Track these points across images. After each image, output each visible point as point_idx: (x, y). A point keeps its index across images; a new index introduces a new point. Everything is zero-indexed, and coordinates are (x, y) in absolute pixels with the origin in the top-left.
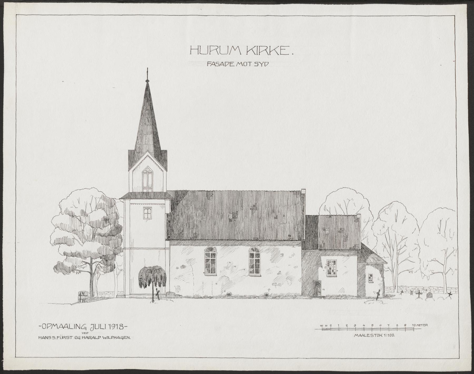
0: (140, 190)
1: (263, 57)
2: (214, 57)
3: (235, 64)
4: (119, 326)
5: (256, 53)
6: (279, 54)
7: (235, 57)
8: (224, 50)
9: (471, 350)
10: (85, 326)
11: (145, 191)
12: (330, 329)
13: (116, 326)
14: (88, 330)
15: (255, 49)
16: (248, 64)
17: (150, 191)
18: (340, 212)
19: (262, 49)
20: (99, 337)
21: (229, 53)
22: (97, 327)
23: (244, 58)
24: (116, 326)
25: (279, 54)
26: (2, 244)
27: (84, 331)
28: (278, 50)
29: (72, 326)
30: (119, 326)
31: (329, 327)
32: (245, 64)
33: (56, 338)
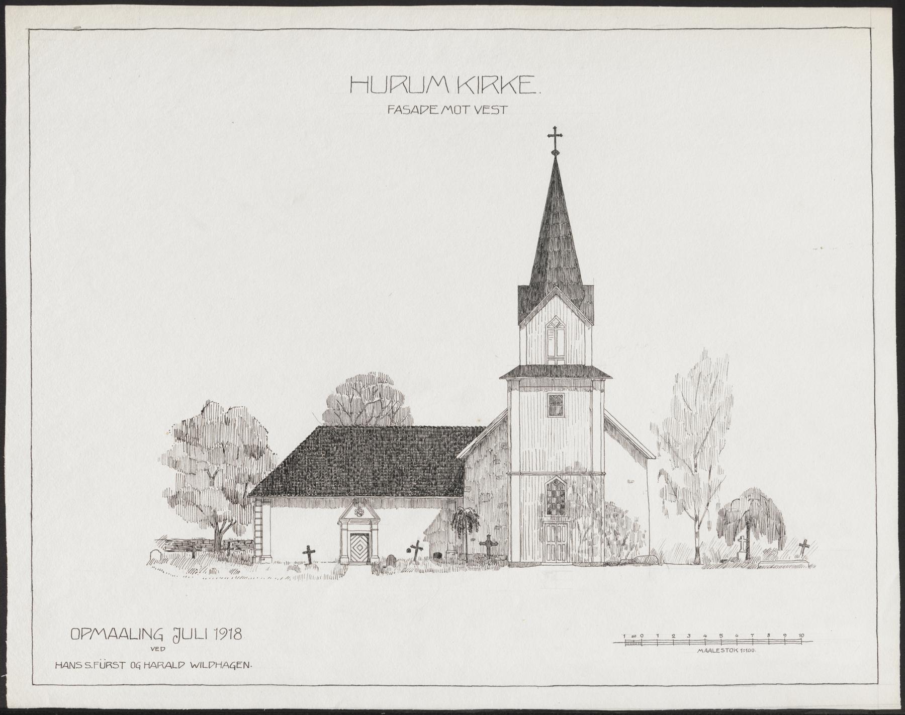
0: (541, 362)
1: (490, 97)
2: (399, 97)
3: (438, 110)
4: (234, 633)
5: (475, 92)
6: (517, 91)
7: (437, 96)
8: (416, 85)
9: (899, 625)
10: (160, 632)
11: (551, 363)
12: (641, 643)
13: (229, 632)
14: (168, 642)
15: (473, 84)
16: (463, 109)
17: (561, 363)
18: (382, 423)
19: (487, 81)
20: (181, 664)
21: (425, 90)
22: (187, 634)
23: (454, 99)
24: (229, 632)
25: (517, 91)
26: (3, 464)
27: (158, 643)
28: (516, 84)
29: (135, 634)
30: (234, 633)
31: (638, 638)
32: (458, 109)
33: (92, 665)
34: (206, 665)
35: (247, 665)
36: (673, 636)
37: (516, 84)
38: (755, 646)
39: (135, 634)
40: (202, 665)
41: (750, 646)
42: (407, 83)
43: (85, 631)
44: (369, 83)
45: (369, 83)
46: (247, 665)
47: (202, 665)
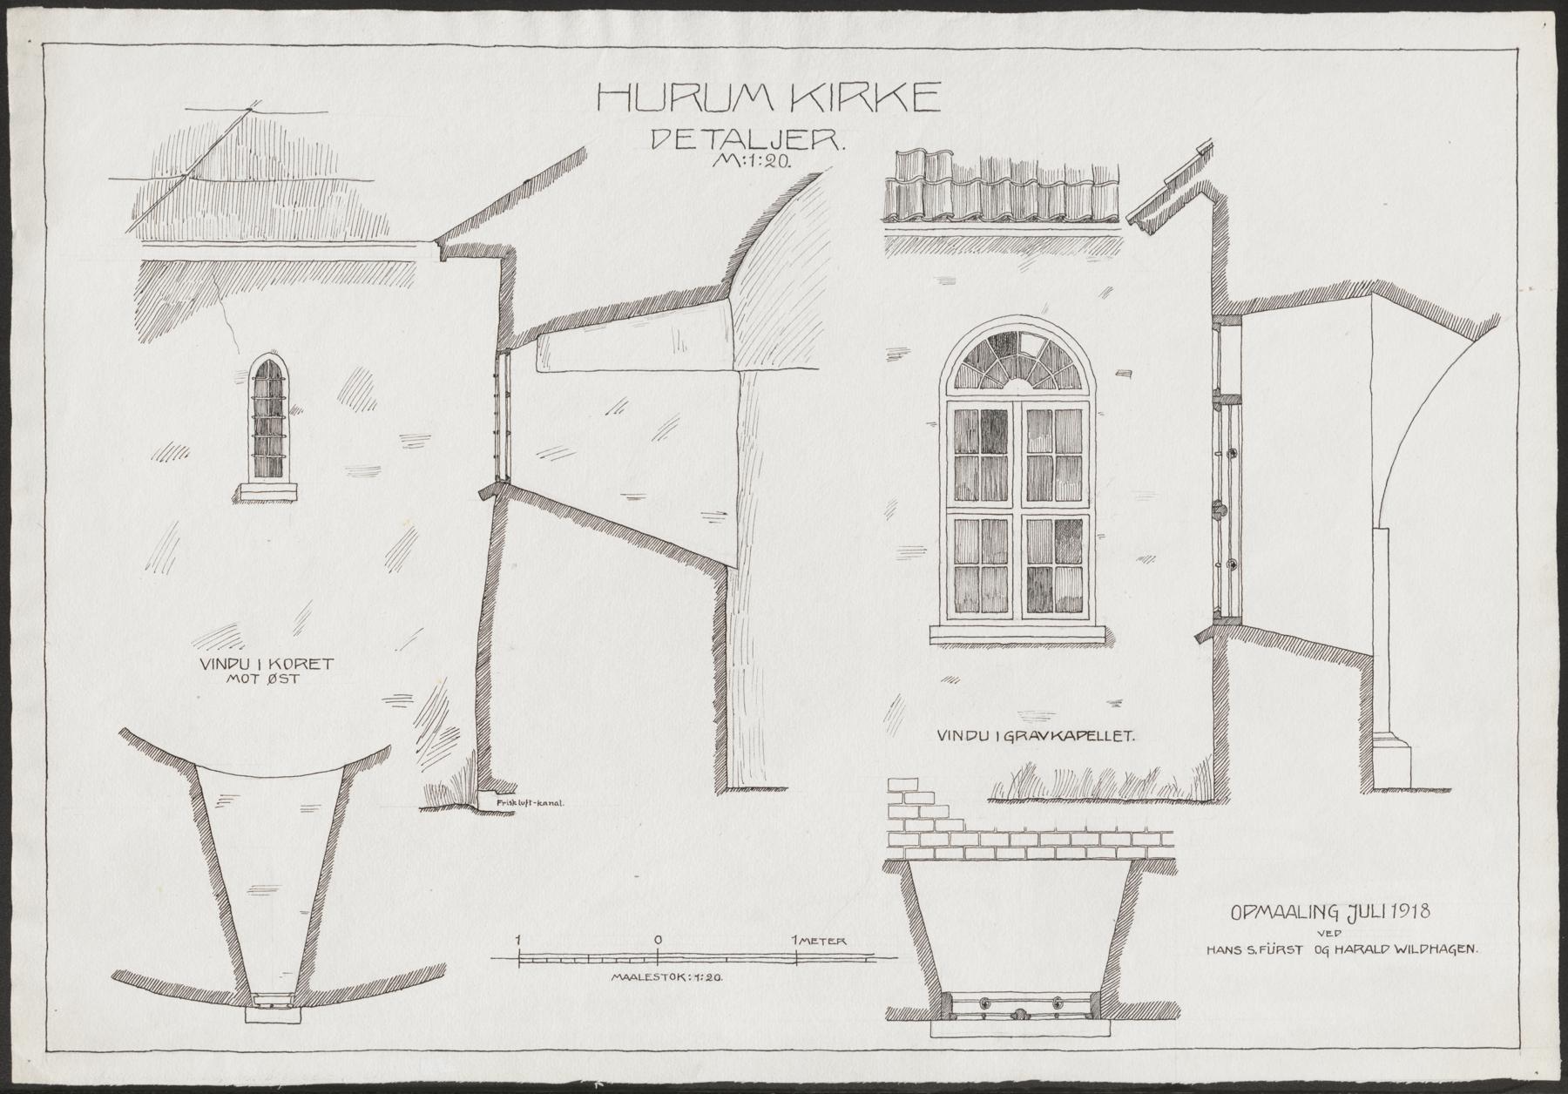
4: (1419, 909)
5: (826, 106)
8: (717, 100)
15: (823, 96)
25: (910, 105)
30: (1419, 909)
34: (1417, 949)
35: (1471, 948)
36: (658, 939)
37: (906, 93)
38: (791, 948)
39: (1305, 912)
40: (1410, 949)
41: (804, 948)
42: (701, 97)
43: (1248, 910)
44: (631, 93)
45: (631, 93)
46: (1471, 948)
47: (1410, 949)
